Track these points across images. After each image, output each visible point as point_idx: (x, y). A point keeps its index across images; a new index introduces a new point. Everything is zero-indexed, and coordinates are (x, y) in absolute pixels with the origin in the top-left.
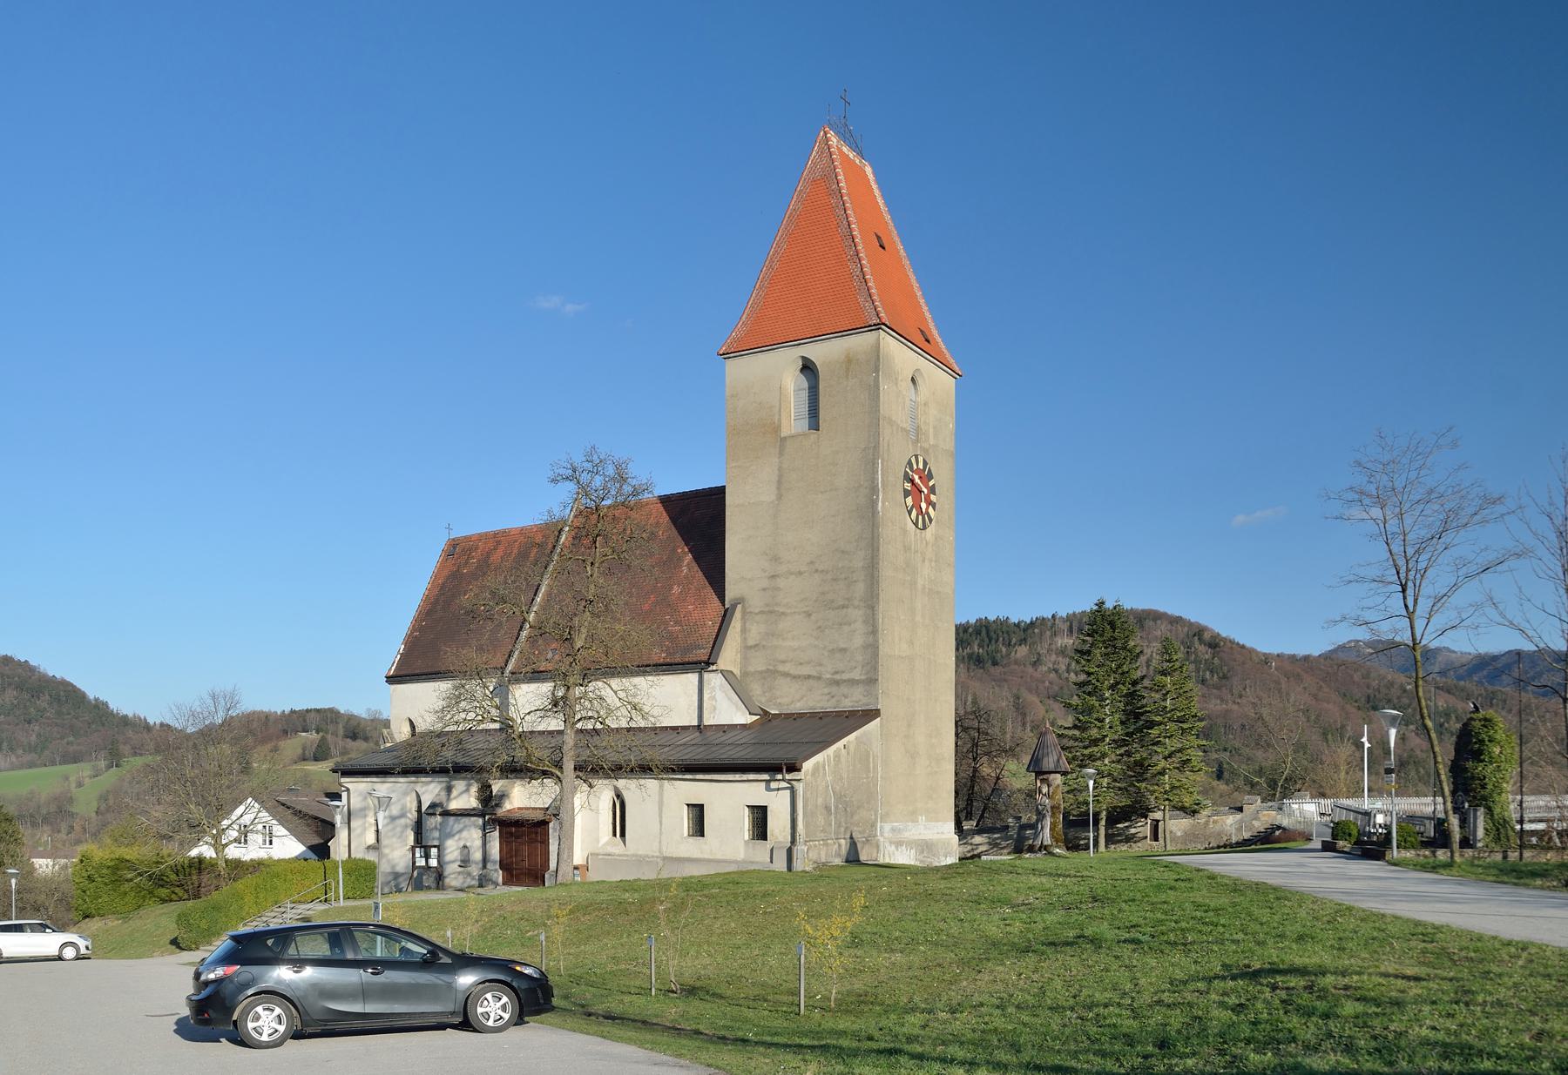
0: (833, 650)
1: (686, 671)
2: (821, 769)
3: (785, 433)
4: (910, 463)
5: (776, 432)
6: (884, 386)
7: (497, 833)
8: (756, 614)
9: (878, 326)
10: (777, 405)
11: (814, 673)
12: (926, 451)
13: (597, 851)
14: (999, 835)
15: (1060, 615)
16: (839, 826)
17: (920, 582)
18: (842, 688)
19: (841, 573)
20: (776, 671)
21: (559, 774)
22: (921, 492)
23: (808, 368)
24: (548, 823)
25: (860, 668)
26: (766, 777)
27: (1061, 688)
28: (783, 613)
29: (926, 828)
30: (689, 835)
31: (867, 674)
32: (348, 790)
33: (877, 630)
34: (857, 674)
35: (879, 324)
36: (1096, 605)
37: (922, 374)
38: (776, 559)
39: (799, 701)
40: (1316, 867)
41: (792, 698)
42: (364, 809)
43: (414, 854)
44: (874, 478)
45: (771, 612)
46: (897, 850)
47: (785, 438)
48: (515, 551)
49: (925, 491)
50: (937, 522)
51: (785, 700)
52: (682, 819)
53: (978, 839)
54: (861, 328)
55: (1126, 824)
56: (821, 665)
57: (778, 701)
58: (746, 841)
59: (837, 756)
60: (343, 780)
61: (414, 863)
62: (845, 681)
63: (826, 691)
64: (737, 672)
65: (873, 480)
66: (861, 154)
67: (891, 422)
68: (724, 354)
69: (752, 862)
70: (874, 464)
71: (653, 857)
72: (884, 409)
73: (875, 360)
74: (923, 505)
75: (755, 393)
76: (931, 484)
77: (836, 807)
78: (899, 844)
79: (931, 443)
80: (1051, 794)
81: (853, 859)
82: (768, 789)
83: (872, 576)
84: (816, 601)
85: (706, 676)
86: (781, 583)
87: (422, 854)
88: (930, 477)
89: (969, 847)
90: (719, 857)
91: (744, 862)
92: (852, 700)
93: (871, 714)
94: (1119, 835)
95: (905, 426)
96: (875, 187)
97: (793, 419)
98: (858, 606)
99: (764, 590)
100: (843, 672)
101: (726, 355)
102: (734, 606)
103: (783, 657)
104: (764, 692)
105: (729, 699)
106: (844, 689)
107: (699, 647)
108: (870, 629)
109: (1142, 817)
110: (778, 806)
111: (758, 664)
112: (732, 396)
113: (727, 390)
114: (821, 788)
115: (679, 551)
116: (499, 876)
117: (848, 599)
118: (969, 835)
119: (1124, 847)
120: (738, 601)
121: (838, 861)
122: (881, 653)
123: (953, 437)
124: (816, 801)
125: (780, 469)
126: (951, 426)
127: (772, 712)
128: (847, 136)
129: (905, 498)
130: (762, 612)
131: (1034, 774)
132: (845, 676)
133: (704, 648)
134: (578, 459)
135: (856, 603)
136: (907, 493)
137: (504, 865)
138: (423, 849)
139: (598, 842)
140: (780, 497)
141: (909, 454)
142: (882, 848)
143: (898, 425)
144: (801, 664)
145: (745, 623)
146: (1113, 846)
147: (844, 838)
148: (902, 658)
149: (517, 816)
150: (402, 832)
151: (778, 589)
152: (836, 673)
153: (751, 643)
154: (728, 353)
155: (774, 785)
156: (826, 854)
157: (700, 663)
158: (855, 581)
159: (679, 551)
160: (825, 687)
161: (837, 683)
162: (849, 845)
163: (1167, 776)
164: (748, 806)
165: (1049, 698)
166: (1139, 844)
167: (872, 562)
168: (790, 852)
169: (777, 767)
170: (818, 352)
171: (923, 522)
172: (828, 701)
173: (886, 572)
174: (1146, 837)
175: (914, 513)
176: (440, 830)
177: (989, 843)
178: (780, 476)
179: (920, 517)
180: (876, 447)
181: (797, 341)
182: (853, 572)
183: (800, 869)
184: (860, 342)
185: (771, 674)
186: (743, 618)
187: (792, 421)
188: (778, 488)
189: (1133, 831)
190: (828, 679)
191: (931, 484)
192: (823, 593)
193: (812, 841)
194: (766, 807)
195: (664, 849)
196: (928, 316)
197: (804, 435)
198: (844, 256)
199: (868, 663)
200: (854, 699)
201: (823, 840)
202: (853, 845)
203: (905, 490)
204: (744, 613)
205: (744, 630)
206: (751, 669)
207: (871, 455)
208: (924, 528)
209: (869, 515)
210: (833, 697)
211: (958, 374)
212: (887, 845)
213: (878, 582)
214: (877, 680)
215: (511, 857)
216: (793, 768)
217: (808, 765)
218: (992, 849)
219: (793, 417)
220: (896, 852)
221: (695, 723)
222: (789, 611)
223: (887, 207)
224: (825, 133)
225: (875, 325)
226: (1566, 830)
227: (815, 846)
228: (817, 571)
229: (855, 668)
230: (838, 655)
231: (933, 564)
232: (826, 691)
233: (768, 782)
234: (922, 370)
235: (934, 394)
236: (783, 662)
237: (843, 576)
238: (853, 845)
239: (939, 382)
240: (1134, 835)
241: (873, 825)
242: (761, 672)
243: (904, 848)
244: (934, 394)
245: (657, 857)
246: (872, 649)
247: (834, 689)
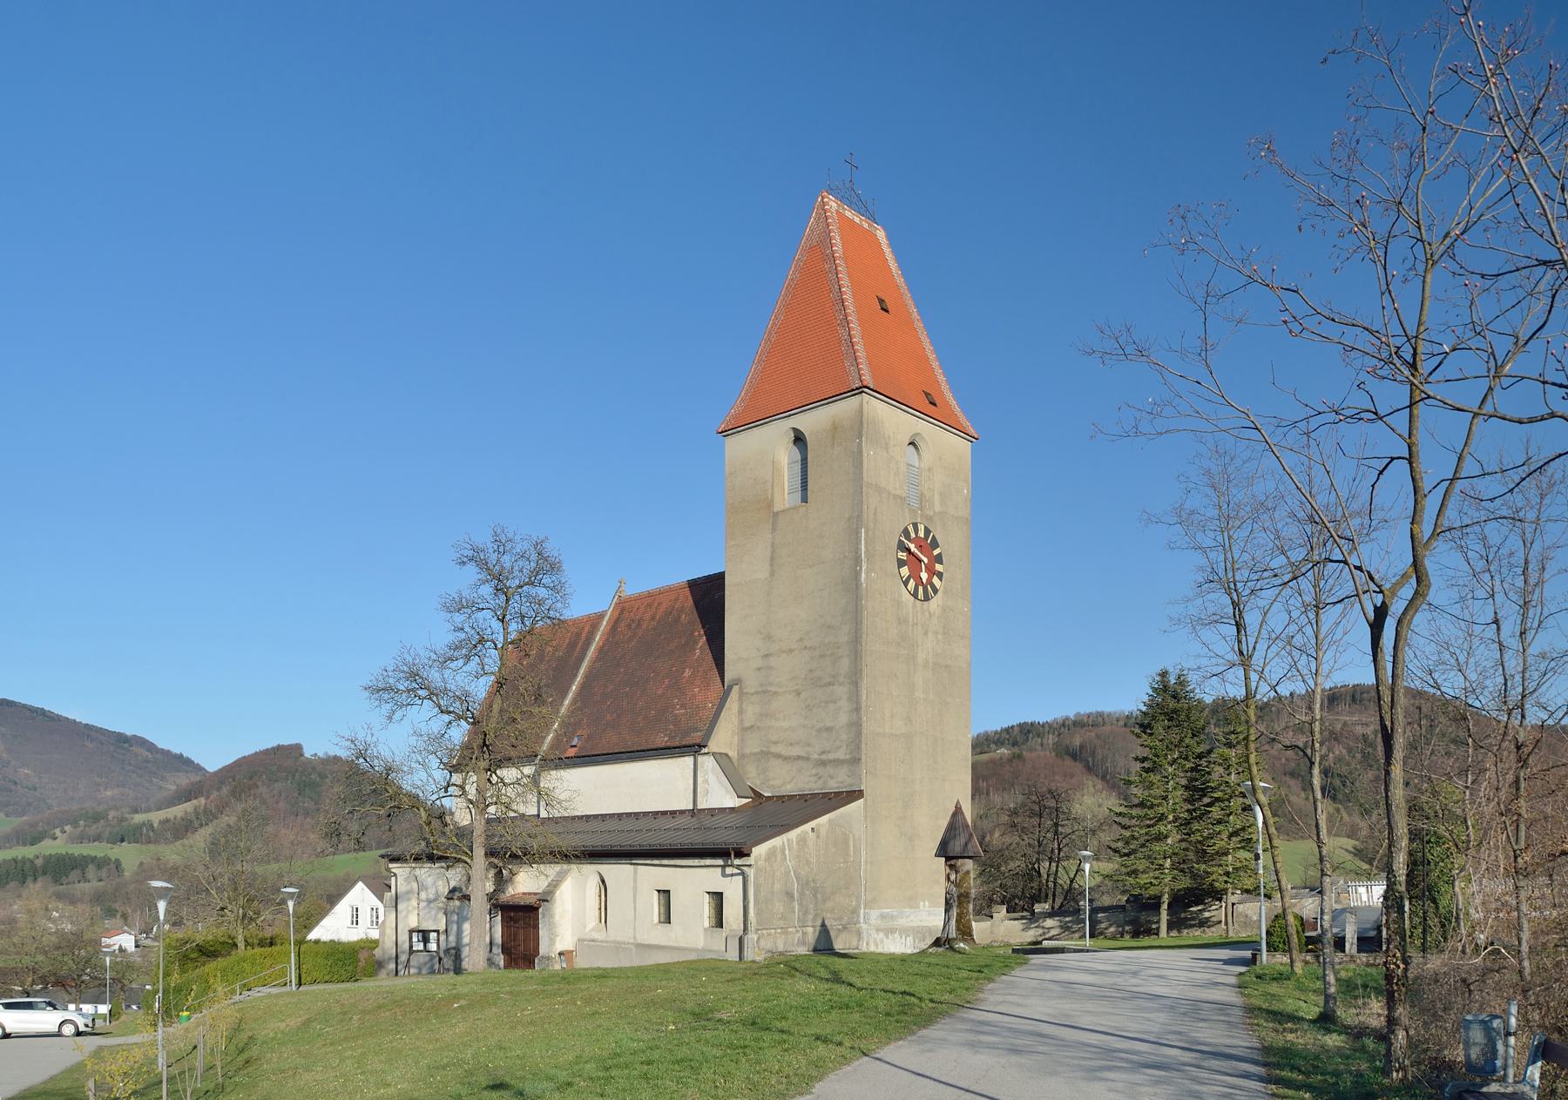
0: (820, 729)
1: (682, 755)
2: (779, 856)
3: (777, 507)
4: (906, 533)
5: (769, 507)
6: (869, 452)
7: (499, 918)
8: (752, 694)
9: (861, 389)
10: (771, 480)
11: (803, 754)
12: (930, 519)
13: (584, 937)
14: (1070, 918)
15: (1298, 692)
16: (806, 913)
17: (921, 656)
18: (828, 768)
19: (828, 649)
20: (769, 753)
21: (469, 861)
22: (920, 561)
23: (799, 439)
24: (537, 909)
25: (845, 747)
26: (720, 862)
27: (1298, 765)
28: (776, 693)
29: (929, 914)
30: (660, 922)
31: (850, 753)
32: (395, 875)
33: (861, 708)
34: (841, 754)
35: (861, 388)
36: (1160, 675)
37: (923, 437)
38: (769, 638)
39: (790, 782)
40: (1224, 970)
41: (782, 780)
42: (408, 892)
43: (411, 938)
44: (857, 548)
45: (764, 692)
46: (888, 938)
47: (777, 513)
48: (567, 641)
49: (926, 560)
50: (945, 592)
51: (777, 782)
52: (652, 905)
53: (1049, 923)
54: (845, 393)
55: (1200, 908)
56: (809, 745)
57: (771, 783)
58: (705, 929)
59: (802, 840)
60: (391, 866)
61: (411, 947)
62: (831, 761)
63: (814, 772)
64: (733, 754)
65: (857, 550)
66: (873, 219)
67: (879, 489)
68: (722, 432)
69: (709, 951)
70: (857, 533)
71: (628, 943)
72: (868, 476)
73: (859, 426)
74: (924, 576)
75: (751, 469)
76: (936, 552)
77: (802, 894)
78: (889, 931)
79: (937, 510)
80: (958, 881)
81: (824, 945)
82: (724, 875)
83: (856, 652)
84: (805, 679)
85: (700, 758)
86: (773, 661)
87: (420, 938)
88: (935, 544)
89: (1041, 931)
90: (683, 945)
91: (703, 950)
92: (838, 781)
93: (854, 795)
94: (1193, 919)
95: (899, 492)
96: (887, 251)
97: (785, 494)
98: (843, 683)
99: (759, 669)
100: (829, 752)
101: (725, 433)
102: (730, 688)
103: (775, 738)
104: (759, 774)
105: (720, 782)
106: (830, 770)
107: (696, 730)
108: (854, 706)
109: (1217, 900)
110: (732, 890)
111: (753, 746)
112: (731, 474)
113: (727, 468)
114: (778, 874)
115: (696, 634)
116: (500, 960)
117: (834, 676)
118: (1041, 918)
119: (1197, 932)
120: (737, 682)
121: (803, 950)
122: (864, 731)
123: (968, 504)
124: (772, 887)
125: (773, 544)
126: (965, 491)
127: (766, 795)
128: (849, 197)
129: (899, 568)
130: (757, 693)
131: (944, 859)
132: (831, 756)
133: (700, 731)
134: (484, 539)
135: (842, 679)
136: (901, 563)
137: (506, 949)
138: (420, 934)
139: (585, 927)
140: (772, 574)
141: (906, 521)
142: (865, 935)
143: (889, 493)
144: (791, 744)
145: (742, 704)
146: (1186, 931)
147: (813, 926)
148: (896, 736)
149: (517, 901)
150: (436, 915)
151: (770, 668)
152: (823, 753)
153: (747, 724)
154: (726, 431)
155: (729, 870)
156: (785, 943)
157: (694, 746)
158: (840, 657)
159: (696, 634)
160: (812, 768)
161: (823, 763)
162: (817, 933)
163: (1230, 856)
164: (708, 893)
165: (1285, 774)
166: (1213, 929)
167: (856, 637)
168: (741, 940)
169: (728, 853)
170: (807, 422)
171: (926, 593)
172: (816, 782)
173: (872, 645)
174: (1221, 921)
175: (912, 584)
176: (458, 914)
177: (1061, 927)
178: (773, 552)
179: (921, 588)
180: (859, 517)
181: (787, 413)
182: (838, 648)
183: (750, 959)
184: (843, 408)
185: (765, 755)
186: (740, 699)
187: (786, 495)
188: (771, 565)
189: (1207, 914)
190: (815, 759)
191: (936, 552)
192: (811, 671)
193: (767, 929)
194: (669, 891)
195: (638, 937)
196: (941, 378)
197: (795, 508)
198: (834, 321)
199: (852, 742)
200: (839, 780)
201: (782, 928)
202: (824, 931)
203: (899, 560)
204: (741, 694)
205: (741, 712)
206: (747, 751)
207: (855, 523)
208: (927, 598)
209: (853, 588)
210: (820, 778)
211: (974, 437)
212: (873, 932)
213: (861, 658)
214: (861, 759)
215: (511, 941)
216: (741, 854)
217: (759, 851)
218: (1064, 932)
219: (786, 492)
220: (885, 940)
221: (690, 807)
222: (781, 691)
223: (901, 270)
224: (823, 198)
225: (857, 389)
226: (1559, 926)
227: (769, 935)
228: (806, 648)
229: (841, 747)
230: (825, 735)
231: (940, 637)
232: (814, 772)
233: (723, 867)
234: (924, 435)
235: (940, 458)
236: (776, 743)
237: (829, 653)
238: (824, 931)
239: (962, 446)
240: (1208, 919)
241: (855, 911)
242: (755, 754)
243: (897, 935)
244: (940, 458)
245: (632, 944)
246: (856, 726)
247: (821, 770)
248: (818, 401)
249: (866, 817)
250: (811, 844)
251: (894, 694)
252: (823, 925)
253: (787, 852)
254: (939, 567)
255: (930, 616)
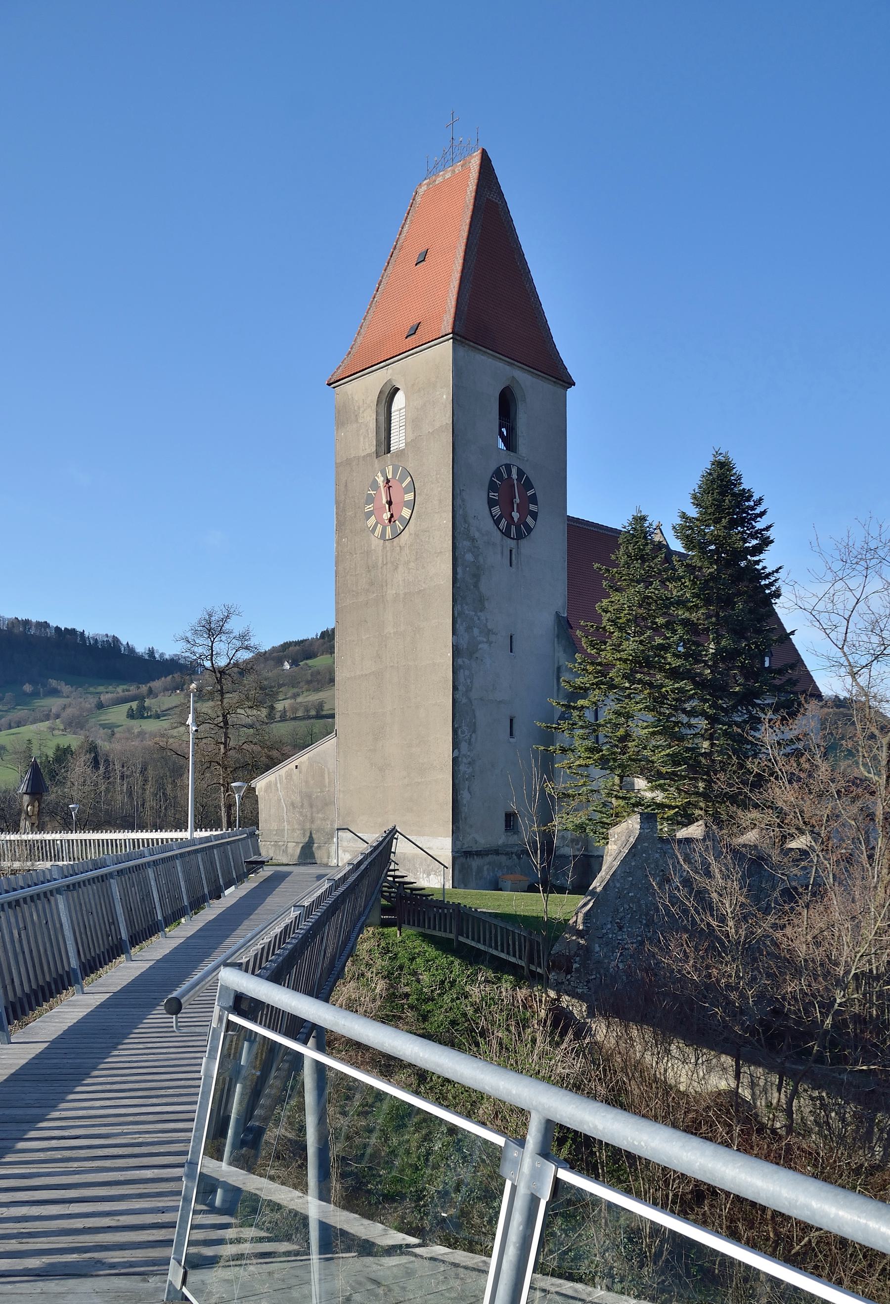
2: (273, 788)
59: (289, 775)
74: (516, 515)
76: (529, 493)
175: (503, 523)
179: (513, 528)
191: (529, 493)
208: (520, 537)
248: (436, 339)
249: (338, 753)
250: (295, 778)
251: (364, 638)
252: (311, 837)
253: (279, 785)
254: (532, 507)
255: (401, 549)
